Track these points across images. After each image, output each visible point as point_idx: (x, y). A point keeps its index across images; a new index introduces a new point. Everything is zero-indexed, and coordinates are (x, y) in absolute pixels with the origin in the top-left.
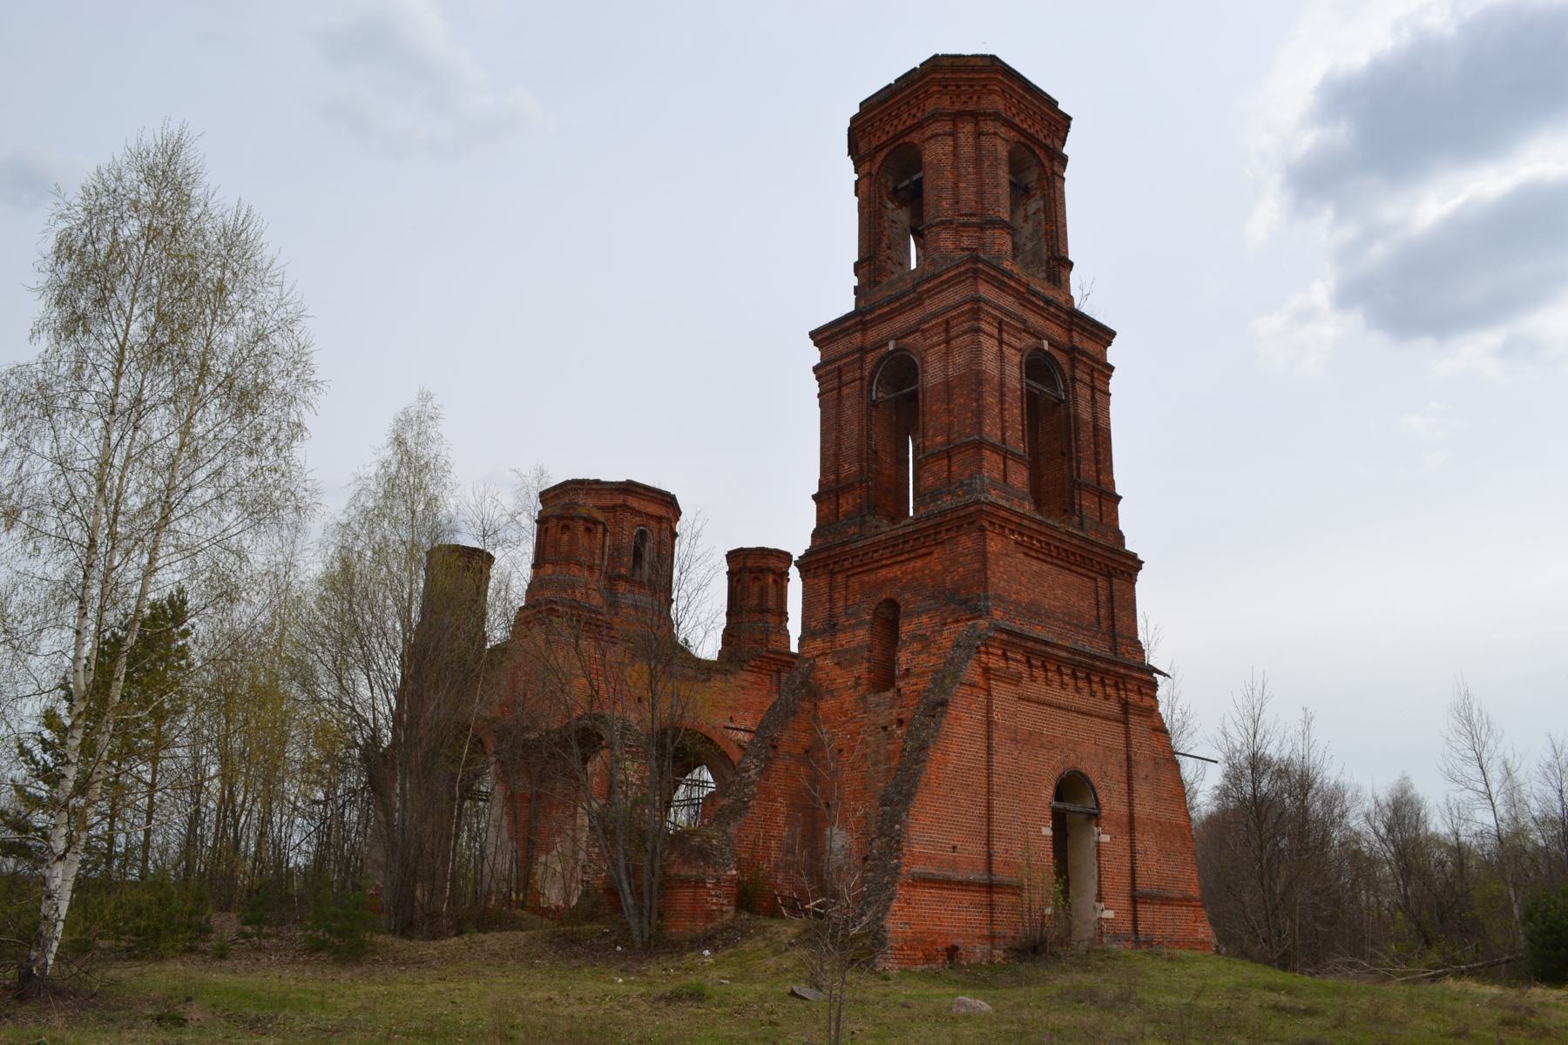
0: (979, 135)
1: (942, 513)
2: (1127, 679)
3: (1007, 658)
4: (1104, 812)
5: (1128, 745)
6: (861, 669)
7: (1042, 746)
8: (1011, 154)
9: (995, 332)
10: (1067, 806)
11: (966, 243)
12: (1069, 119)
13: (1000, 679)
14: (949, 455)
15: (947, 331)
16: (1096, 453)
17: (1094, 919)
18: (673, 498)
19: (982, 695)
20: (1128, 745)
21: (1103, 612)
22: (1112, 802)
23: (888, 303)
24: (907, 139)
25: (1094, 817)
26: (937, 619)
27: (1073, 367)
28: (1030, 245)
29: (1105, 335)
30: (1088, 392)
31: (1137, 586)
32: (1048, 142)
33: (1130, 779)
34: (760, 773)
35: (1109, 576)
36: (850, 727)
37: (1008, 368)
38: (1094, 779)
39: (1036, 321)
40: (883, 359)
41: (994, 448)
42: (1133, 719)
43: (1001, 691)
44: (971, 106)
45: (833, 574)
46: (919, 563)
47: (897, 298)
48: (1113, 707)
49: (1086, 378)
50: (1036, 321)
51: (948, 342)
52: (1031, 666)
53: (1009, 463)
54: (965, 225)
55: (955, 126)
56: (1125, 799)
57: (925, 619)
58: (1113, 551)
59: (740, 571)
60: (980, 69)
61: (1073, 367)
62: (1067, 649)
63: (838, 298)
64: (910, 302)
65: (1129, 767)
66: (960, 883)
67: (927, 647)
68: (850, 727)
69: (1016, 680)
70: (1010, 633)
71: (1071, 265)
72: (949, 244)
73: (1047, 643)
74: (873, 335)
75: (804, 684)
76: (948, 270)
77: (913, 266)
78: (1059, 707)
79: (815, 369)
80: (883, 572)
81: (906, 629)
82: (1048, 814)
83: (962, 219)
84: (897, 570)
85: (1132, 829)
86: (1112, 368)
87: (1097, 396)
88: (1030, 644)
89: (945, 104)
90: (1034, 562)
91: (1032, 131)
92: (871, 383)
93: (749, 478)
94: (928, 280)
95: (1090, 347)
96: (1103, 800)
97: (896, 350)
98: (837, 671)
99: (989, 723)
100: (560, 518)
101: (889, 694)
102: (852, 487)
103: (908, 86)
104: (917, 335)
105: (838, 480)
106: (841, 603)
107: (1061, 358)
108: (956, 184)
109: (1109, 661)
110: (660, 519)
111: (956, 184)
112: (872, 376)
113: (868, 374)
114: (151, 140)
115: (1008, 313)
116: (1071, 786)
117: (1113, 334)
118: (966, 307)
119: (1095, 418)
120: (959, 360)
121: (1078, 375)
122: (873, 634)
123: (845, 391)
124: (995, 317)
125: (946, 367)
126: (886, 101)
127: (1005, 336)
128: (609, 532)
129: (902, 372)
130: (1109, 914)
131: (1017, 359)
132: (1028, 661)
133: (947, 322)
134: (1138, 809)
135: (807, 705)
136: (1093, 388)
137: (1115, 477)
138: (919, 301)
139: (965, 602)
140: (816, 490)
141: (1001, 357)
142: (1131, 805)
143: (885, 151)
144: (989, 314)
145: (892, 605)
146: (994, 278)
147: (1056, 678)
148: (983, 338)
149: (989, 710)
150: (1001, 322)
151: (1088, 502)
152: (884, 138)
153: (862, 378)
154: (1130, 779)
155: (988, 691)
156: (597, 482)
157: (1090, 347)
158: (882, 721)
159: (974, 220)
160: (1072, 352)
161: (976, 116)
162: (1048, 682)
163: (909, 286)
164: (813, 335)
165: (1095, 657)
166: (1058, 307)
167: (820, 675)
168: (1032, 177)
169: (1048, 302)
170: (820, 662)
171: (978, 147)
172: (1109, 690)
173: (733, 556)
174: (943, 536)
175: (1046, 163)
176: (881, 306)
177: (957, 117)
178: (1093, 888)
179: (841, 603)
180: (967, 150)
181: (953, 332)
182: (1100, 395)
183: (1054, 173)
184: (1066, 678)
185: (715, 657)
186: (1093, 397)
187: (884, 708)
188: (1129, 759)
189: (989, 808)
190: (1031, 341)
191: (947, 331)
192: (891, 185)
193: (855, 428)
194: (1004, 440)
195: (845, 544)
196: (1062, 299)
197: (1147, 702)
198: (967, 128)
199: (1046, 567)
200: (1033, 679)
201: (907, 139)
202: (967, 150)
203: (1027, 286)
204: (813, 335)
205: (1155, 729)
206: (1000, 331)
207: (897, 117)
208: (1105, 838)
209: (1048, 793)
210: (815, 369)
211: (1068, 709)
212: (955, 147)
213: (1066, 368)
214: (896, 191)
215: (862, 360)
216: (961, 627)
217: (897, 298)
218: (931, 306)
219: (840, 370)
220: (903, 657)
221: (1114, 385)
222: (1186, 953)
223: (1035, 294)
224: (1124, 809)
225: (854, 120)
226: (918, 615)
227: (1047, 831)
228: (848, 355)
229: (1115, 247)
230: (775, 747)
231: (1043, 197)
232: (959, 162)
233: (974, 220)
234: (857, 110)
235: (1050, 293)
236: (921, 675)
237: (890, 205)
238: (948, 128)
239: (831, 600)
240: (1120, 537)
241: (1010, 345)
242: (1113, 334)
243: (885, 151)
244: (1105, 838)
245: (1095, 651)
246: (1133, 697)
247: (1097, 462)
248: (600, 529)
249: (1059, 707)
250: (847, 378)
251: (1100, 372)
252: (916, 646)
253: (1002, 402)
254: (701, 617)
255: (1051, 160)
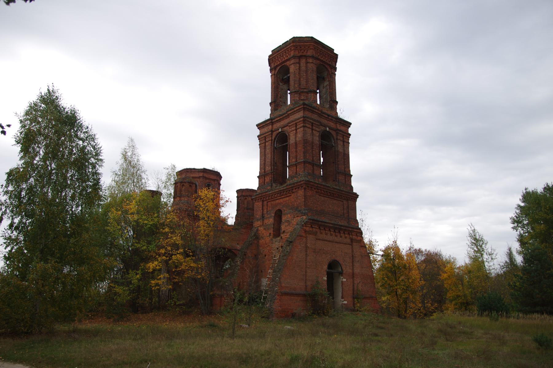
0: (307, 63)
1: (294, 184)
2: (354, 231)
3: (312, 228)
4: (344, 272)
5: (353, 251)
6: (271, 231)
7: (324, 253)
8: (317, 68)
9: (311, 127)
10: (332, 271)
11: (302, 98)
12: (337, 55)
13: (310, 234)
14: (296, 165)
15: (296, 126)
16: (344, 162)
17: (341, 303)
18: (219, 173)
19: (304, 239)
20: (353, 251)
21: (345, 211)
22: (347, 269)
23: (279, 117)
24: (285, 64)
25: (341, 273)
26: (292, 216)
27: (337, 135)
28: (325, 96)
29: (348, 124)
30: (342, 143)
31: (357, 203)
32: (330, 63)
33: (353, 262)
34: (241, 263)
35: (348, 200)
36: (268, 248)
37: (315, 137)
38: (341, 262)
39: (325, 122)
40: (278, 134)
41: (309, 163)
42: (354, 244)
43: (311, 238)
44: (304, 54)
45: (263, 201)
46: (287, 199)
47: (282, 115)
48: (348, 241)
49: (341, 138)
50: (325, 122)
51: (296, 130)
52: (320, 229)
53: (315, 167)
54: (302, 92)
55: (300, 60)
56: (351, 268)
57: (289, 215)
58: (350, 193)
59: (240, 196)
60: (308, 42)
61: (337, 135)
62: (332, 224)
63: (265, 114)
64: (286, 116)
65: (353, 258)
66: (297, 294)
67: (289, 224)
68: (268, 248)
69: (315, 234)
70: (313, 220)
71: (337, 102)
72: (297, 98)
73: (325, 222)
74: (276, 126)
75: (254, 235)
76: (296, 107)
77: (289, 103)
78: (329, 241)
79: (258, 136)
80: (278, 201)
81: (284, 218)
82: (325, 273)
83: (302, 90)
84: (281, 200)
85: (353, 277)
86: (350, 135)
87: (345, 144)
88: (320, 223)
89: (297, 53)
90: (322, 197)
91: (324, 60)
92: (274, 142)
93: (241, 171)
94: (290, 110)
95: (343, 128)
96: (344, 269)
97: (281, 131)
98: (264, 231)
99: (306, 247)
100: (181, 182)
101: (279, 238)
102: (272, 171)
103: (286, 47)
104: (288, 127)
105: (265, 172)
106: (265, 210)
107: (333, 133)
108: (300, 79)
109: (346, 227)
110: (214, 180)
111: (300, 79)
112: (275, 139)
113: (274, 140)
114: (44, 91)
115: (314, 120)
116: (333, 265)
117: (351, 124)
118: (302, 119)
119: (344, 151)
120: (299, 136)
121: (339, 137)
122: (275, 220)
123: (267, 144)
124: (310, 122)
125: (296, 137)
126: (279, 51)
127: (314, 128)
128: (198, 183)
129: (283, 138)
130: (346, 302)
131: (318, 135)
132: (319, 228)
133: (343, 136)
134: (355, 271)
135: (256, 242)
136: (344, 142)
137: (351, 169)
138: (288, 116)
139: (300, 211)
140: (258, 175)
141: (312, 134)
142: (353, 270)
143: (279, 68)
144: (308, 121)
145: (280, 211)
146: (311, 110)
147: (329, 232)
148: (306, 129)
149: (306, 244)
150: (312, 123)
151: (341, 178)
152: (278, 63)
153: (272, 140)
154: (353, 262)
155: (306, 237)
156: (194, 169)
157: (343, 128)
158: (277, 247)
159: (305, 90)
160: (337, 131)
161: (306, 57)
162: (326, 234)
163: (285, 112)
164: (257, 125)
165: (342, 226)
166: (332, 117)
167: (260, 232)
168: (325, 74)
169: (329, 116)
170: (259, 228)
171: (306, 67)
172: (346, 235)
173: (238, 191)
174: (294, 190)
175: (330, 70)
176: (277, 118)
177: (300, 57)
178: (340, 295)
179: (265, 210)
180: (303, 68)
181: (298, 127)
182: (346, 144)
183: (332, 73)
184: (332, 233)
185: (233, 224)
186: (344, 144)
187: (277, 243)
188: (353, 256)
189: (306, 272)
190: (323, 128)
191: (296, 126)
192: (281, 77)
193: (270, 155)
194: (313, 161)
195: (266, 192)
196: (334, 114)
197: (359, 238)
198: (303, 61)
199: (326, 199)
200: (321, 233)
201: (285, 64)
202: (303, 68)
203: (322, 112)
204: (257, 125)
205: (362, 246)
206: (312, 126)
207: (282, 56)
208: (345, 280)
209: (325, 267)
210: (258, 136)
211: (332, 242)
212: (300, 67)
213: (335, 136)
214: (283, 79)
215: (272, 134)
216: (299, 219)
217: (282, 115)
218: (292, 118)
219: (265, 137)
220: (283, 227)
221: (351, 140)
222: (104, 325)
223: (324, 113)
224: (351, 271)
225: (270, 56)
226: (287, 214)
227: (325, 278)
228: (268, 132)
229: (354, 95)
230: (245, 255)
231: (329, 81)
232: (304, 70)
233: (305, 90)
234: (271, 53)
235: (329, 113)
236: (287, 233)
237: (281, 84)
238: (297, 61)
239: (263, 209)
240: (352, 188)
241: (316, 130)
242: (351, 124)
243: (279, 68)
244: (345, 280)
245: (343, 224)
246: (354, 237)
247: (345, 165)
248: (194, 185)
249: (329, 241)
250: (267, 140)
251: (346, 136)
252: (286, 224)
253: (312, 148)
254: (229, 212)
255: (331, 69)
